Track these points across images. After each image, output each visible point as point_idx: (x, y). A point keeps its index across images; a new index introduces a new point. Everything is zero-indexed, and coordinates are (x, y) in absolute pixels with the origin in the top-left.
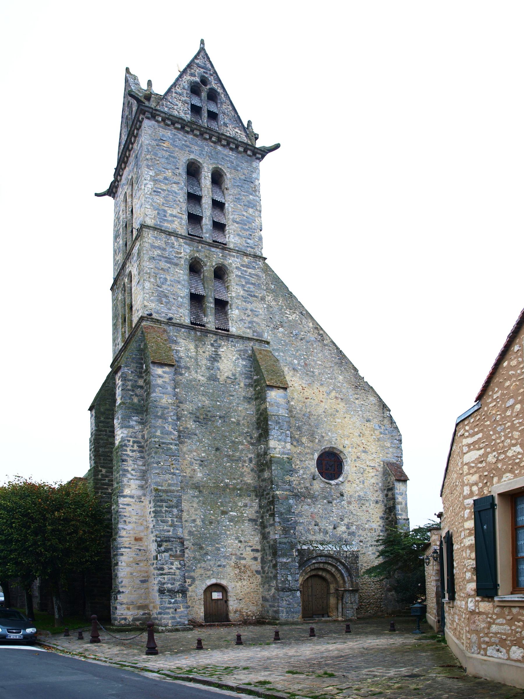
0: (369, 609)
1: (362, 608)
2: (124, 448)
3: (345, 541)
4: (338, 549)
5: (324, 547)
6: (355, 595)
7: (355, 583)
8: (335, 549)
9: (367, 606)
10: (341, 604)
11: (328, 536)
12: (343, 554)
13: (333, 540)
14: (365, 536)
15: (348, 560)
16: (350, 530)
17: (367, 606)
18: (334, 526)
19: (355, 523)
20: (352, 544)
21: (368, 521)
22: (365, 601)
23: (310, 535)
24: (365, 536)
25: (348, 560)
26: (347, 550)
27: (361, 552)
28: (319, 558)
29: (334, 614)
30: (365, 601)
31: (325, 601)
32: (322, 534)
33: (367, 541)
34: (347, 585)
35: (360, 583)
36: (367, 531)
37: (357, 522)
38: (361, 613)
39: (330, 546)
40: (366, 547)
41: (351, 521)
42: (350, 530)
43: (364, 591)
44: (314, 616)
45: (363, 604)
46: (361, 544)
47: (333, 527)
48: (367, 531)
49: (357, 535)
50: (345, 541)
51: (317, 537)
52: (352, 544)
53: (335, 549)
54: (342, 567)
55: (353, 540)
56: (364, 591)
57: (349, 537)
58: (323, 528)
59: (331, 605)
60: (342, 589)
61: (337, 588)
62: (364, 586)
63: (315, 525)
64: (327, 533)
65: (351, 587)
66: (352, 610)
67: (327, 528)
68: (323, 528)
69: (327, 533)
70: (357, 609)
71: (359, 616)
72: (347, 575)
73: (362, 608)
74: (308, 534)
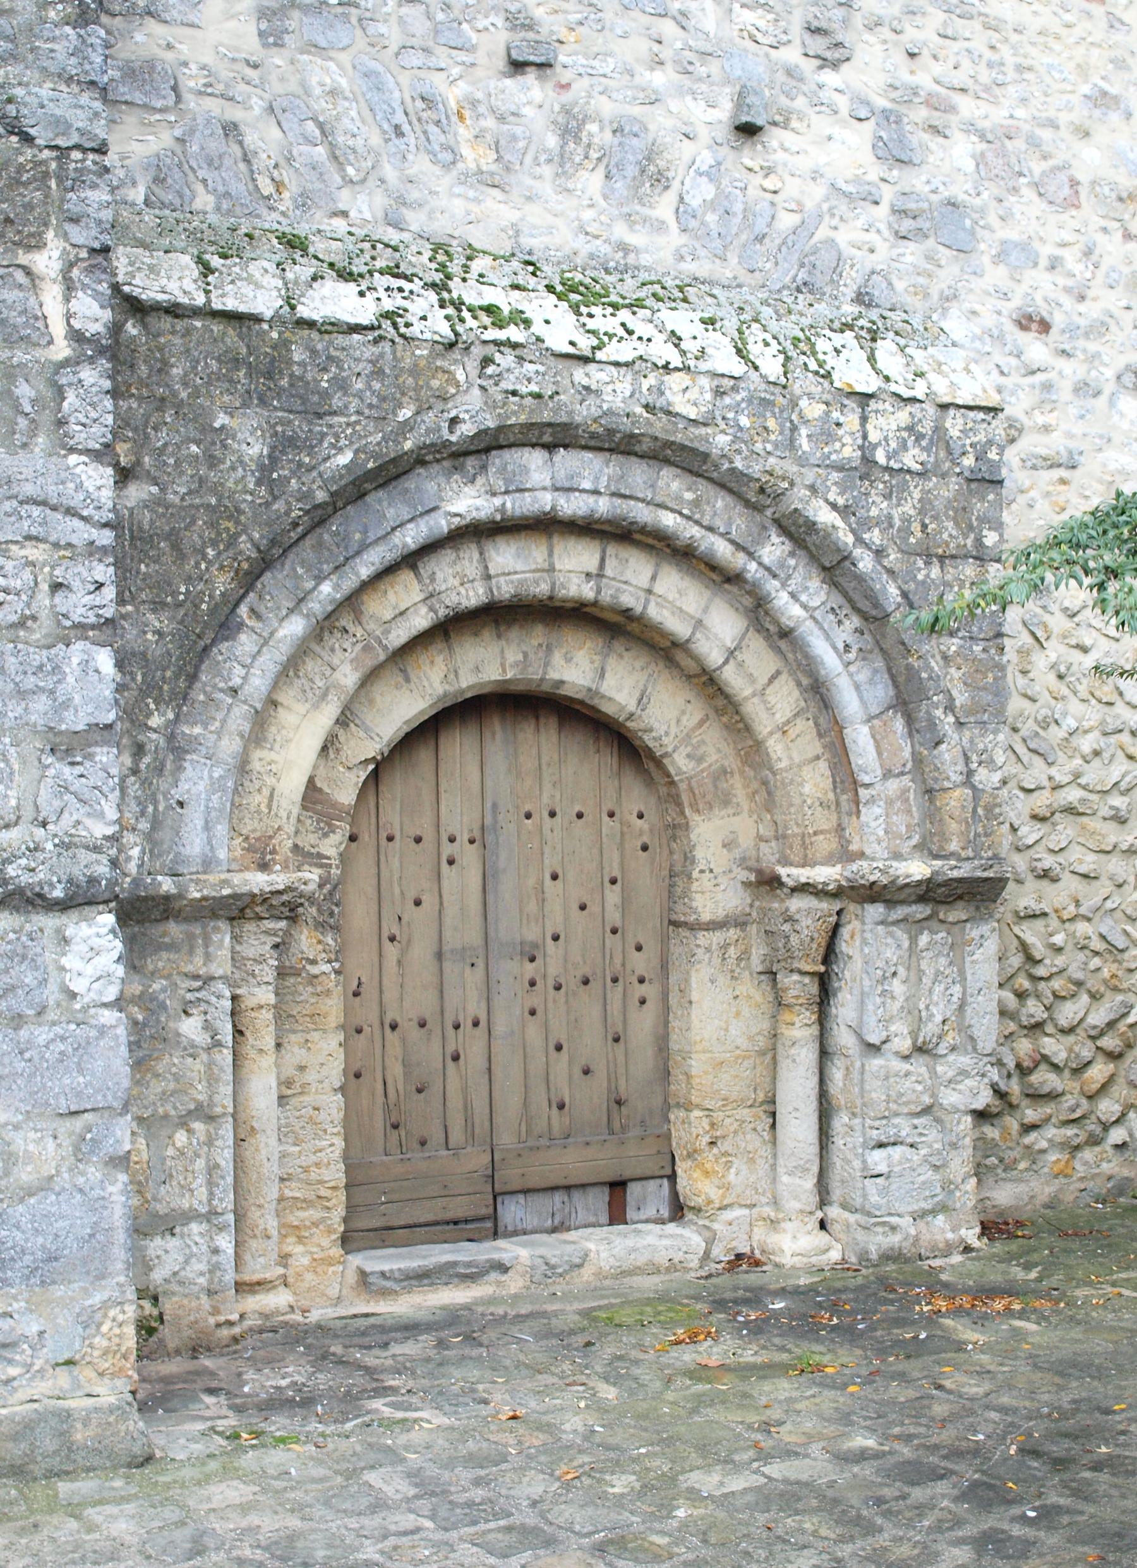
0: (1108, 1107)
1: (1037, 1097)
2: (997, 810)
3: (862, 298)
4: (772, 367)
5: (603, 321)
6: (957, 950)
7: (956, 800)
8: (726, 362)
9: (1098, 1072)
10: (806, 1056)
11: (664, 208)
12: (827, 433)
13: (726, 273)
14: (1071, 259)
15: (878, 506)
16: (917, 181)
17: (1098, 1072)
18: (741, 100)
19: (966, 106)
20: (932, 335)
21: (1103, 100)
22: (1068, 1013)
23: (444, 182)
24: (1071, 259)
25: (878, 506)
26: (868, 383)
27: (1028, 444)
28: (533, 461)
29: (738, 1175)
30: (1068, 1013)
31: (643, 1024)
32: (592, 182)
33: (1099, 329)
34: (873, 816)
35: (1018, 809)
36: (1090, 214)
37: (991, 91)
38: (1034, 1155)
39: (682, 320)
40: (1086, 390)
41: (924, 80)
42: (917, 181)
43: (1056, 896)
44: (512, 1211)
45: (1053, 1046)
46: (1036, 350)
47: (724, 113)
48: (1090, 214)
49: (986, 247)
50: (862, 298)
51: (534, 214)
52: (932, 335)
53: (726, 362)
54: (816, 592)
55: (950, 298)
56: (1056, 896)
57: (912, 253)
58: (606, 107)
59: (697, 1065)
60: (825, 874)
61: (769, 855)
62: (1065, 831)
63: (517, 66)
64: (661, 180)
65: (927, 848)
66: (933, 1136)
67: (660, 123)
68: (606, 107)
69: (661, 180)
70: (982, 1116)
71: (1004, 1195)
72: (881, 692)
73: (1037, 1097)
74: (420, 165)
